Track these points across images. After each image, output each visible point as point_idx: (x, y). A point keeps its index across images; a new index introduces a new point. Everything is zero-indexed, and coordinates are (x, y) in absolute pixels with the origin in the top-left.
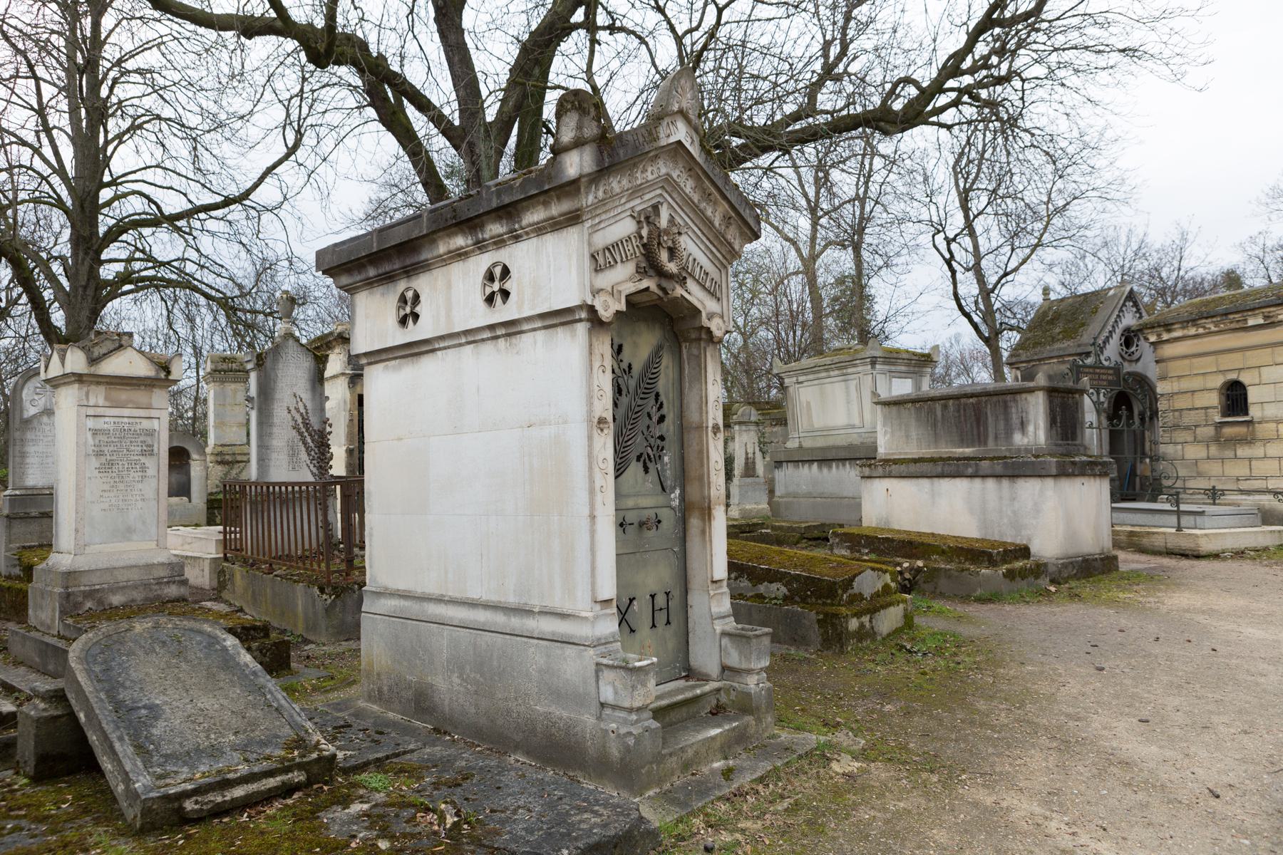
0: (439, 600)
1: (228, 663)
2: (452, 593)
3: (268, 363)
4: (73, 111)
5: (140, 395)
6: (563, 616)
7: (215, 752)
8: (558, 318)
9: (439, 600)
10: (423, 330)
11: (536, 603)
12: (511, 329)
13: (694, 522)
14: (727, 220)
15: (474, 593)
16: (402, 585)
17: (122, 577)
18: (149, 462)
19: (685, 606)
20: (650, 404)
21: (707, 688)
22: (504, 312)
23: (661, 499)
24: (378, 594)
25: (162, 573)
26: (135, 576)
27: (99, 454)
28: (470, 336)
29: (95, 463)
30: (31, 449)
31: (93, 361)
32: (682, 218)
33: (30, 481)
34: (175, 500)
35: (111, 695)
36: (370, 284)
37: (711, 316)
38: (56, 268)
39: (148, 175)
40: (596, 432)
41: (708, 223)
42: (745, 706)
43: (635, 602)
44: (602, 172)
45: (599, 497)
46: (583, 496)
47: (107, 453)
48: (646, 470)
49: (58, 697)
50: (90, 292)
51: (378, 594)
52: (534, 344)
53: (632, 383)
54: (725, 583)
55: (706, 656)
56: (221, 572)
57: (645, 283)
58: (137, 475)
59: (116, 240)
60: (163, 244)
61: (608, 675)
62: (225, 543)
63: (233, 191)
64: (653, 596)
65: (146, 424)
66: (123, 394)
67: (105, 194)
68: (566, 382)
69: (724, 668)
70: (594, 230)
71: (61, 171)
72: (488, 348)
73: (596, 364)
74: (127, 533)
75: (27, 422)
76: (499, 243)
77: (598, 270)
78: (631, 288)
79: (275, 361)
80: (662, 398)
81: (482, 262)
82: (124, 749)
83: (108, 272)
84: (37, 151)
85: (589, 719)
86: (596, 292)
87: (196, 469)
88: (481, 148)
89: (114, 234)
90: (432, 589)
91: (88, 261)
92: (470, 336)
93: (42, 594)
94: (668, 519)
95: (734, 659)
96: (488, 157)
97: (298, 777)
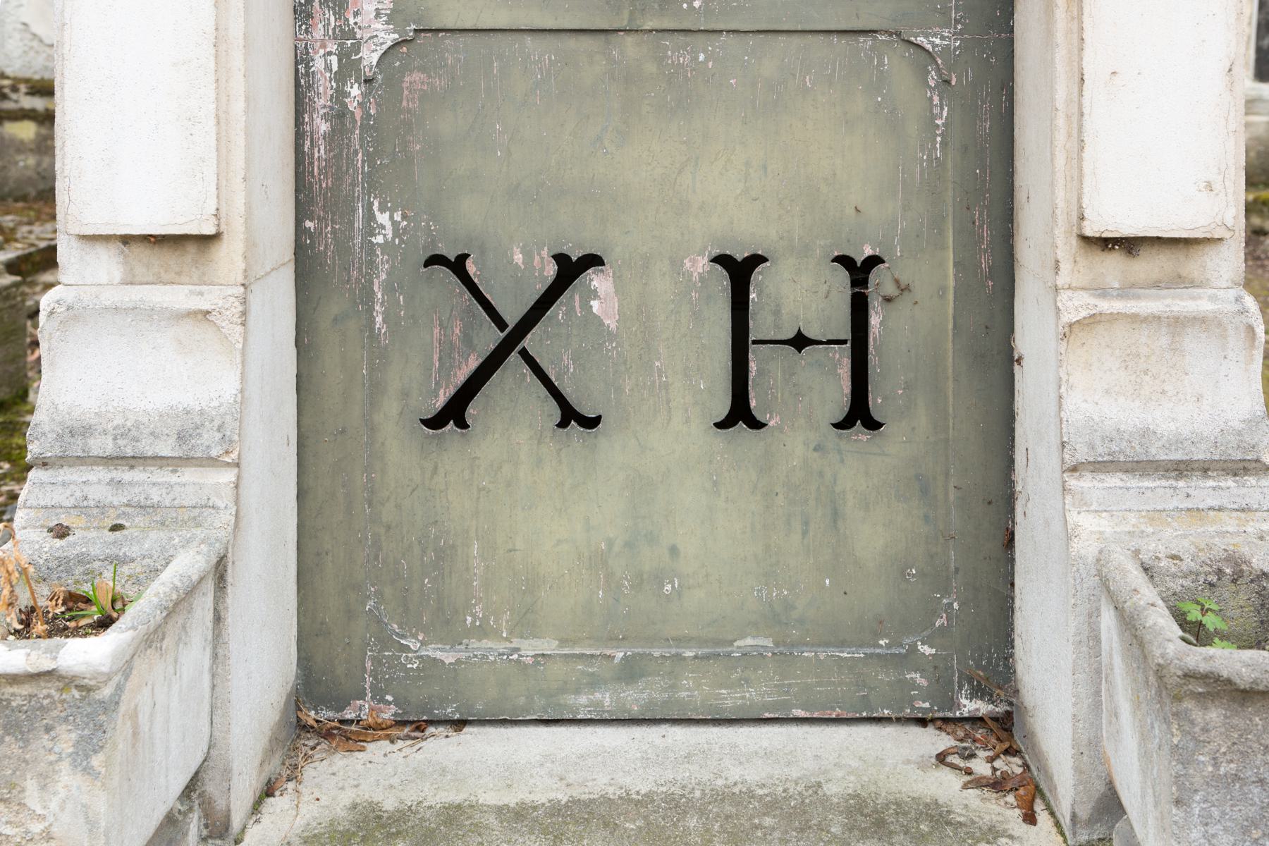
43: (596, 280)
54: (1229, 262)
64: (740, 271)
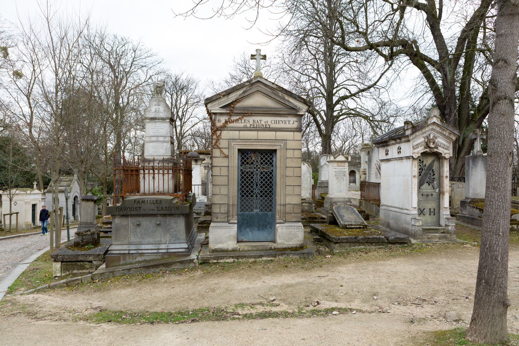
0: (391, 207)
1: (354, 212)
2: (393, 206)
3: (370, 153)
4: (326, 68)
5: (343, 164)
6: (408, 210)
7: (351, 222)
8: (408, 158)
9: (391, 207)
10: (389, 157)
11: (404, 208)
12: (401, 159)
13: (441, 195)
14: (450, 134)
15: (396, 205)
16: (386, 204)
17: (340, 200)
18: (345, 177)
19: (439, 212)
20: (431, 172)
21: (440, 228)
22: (401, 155)
23: (433, 190)
24: (382, 205)
25: (347, 200)
26: (342, 200)
27: (336, 176)
28: (396, 159)
29: (335, 177)
30: (322, 172)
31: (335, 158)
32: (437, 135)
33: (322, 179)
34: (352, 184)
35: (338, 213)
36: (381, 147)
37: (445, 154)
38: (322, 114)
39: (346, 83)
40: (413, 178)
41: (445, 135)
42: (448, 232)
44: (413, 133)
45: (413, 190)
46: (410, 189)
47: (338, 176)
48: (429, 185)
49: (332, 214)
50: (331, 121)
51: (382, 205)
52: (405, 161)
53: (426, 168)
55: (443, 222)
56: (360, 202)
57: (426, 150)
58: (342, 180)
59: (338, 104)
60: (351, 103)
61: (413, 220)
62: (361, 195)
63: (371, 83)
65: (344, 170)
66: (340, 164)
67: (334, 91)
68: (411, 169)
69: (446, 225)
70: (413, 142)
71: (323, 85)
72: (398, 161)
73: (414, 166)
74: (341, 191)
75: (322, 166)
76: (399, 143)
77: (414, 149)
78: (422, 151)
79: (372, 153)
80: (434, 170)
81: (397, 146)
82: (340, 219)
83: (335, 114)
84: (317, 80)
85: (410, 227)
86: (413, 153)
87: (357, 176)
88: (447, 69)
89: (338, 102)
90: (390, 204)
91: (330, 112)
92: (396, 159)
93: (327, 202)
94: (435, 195)
95: (447, 224)
96: (450, 71)
97: (362, 227)
